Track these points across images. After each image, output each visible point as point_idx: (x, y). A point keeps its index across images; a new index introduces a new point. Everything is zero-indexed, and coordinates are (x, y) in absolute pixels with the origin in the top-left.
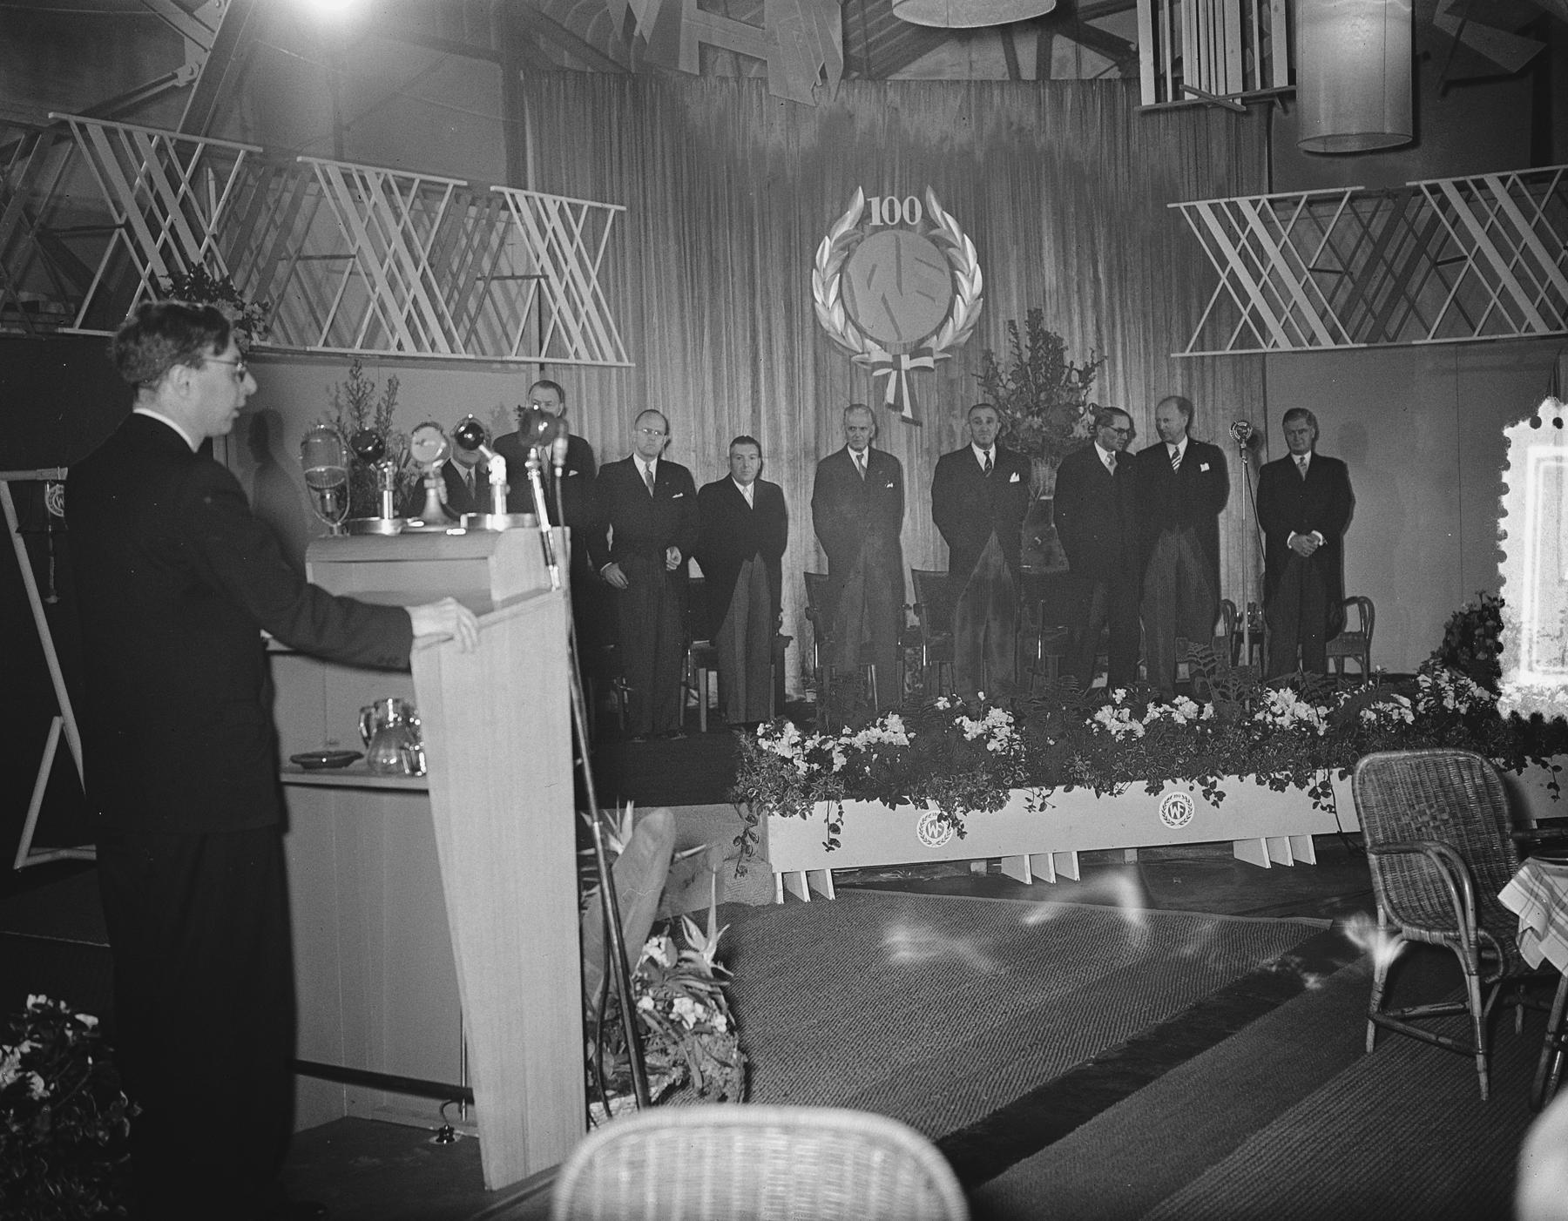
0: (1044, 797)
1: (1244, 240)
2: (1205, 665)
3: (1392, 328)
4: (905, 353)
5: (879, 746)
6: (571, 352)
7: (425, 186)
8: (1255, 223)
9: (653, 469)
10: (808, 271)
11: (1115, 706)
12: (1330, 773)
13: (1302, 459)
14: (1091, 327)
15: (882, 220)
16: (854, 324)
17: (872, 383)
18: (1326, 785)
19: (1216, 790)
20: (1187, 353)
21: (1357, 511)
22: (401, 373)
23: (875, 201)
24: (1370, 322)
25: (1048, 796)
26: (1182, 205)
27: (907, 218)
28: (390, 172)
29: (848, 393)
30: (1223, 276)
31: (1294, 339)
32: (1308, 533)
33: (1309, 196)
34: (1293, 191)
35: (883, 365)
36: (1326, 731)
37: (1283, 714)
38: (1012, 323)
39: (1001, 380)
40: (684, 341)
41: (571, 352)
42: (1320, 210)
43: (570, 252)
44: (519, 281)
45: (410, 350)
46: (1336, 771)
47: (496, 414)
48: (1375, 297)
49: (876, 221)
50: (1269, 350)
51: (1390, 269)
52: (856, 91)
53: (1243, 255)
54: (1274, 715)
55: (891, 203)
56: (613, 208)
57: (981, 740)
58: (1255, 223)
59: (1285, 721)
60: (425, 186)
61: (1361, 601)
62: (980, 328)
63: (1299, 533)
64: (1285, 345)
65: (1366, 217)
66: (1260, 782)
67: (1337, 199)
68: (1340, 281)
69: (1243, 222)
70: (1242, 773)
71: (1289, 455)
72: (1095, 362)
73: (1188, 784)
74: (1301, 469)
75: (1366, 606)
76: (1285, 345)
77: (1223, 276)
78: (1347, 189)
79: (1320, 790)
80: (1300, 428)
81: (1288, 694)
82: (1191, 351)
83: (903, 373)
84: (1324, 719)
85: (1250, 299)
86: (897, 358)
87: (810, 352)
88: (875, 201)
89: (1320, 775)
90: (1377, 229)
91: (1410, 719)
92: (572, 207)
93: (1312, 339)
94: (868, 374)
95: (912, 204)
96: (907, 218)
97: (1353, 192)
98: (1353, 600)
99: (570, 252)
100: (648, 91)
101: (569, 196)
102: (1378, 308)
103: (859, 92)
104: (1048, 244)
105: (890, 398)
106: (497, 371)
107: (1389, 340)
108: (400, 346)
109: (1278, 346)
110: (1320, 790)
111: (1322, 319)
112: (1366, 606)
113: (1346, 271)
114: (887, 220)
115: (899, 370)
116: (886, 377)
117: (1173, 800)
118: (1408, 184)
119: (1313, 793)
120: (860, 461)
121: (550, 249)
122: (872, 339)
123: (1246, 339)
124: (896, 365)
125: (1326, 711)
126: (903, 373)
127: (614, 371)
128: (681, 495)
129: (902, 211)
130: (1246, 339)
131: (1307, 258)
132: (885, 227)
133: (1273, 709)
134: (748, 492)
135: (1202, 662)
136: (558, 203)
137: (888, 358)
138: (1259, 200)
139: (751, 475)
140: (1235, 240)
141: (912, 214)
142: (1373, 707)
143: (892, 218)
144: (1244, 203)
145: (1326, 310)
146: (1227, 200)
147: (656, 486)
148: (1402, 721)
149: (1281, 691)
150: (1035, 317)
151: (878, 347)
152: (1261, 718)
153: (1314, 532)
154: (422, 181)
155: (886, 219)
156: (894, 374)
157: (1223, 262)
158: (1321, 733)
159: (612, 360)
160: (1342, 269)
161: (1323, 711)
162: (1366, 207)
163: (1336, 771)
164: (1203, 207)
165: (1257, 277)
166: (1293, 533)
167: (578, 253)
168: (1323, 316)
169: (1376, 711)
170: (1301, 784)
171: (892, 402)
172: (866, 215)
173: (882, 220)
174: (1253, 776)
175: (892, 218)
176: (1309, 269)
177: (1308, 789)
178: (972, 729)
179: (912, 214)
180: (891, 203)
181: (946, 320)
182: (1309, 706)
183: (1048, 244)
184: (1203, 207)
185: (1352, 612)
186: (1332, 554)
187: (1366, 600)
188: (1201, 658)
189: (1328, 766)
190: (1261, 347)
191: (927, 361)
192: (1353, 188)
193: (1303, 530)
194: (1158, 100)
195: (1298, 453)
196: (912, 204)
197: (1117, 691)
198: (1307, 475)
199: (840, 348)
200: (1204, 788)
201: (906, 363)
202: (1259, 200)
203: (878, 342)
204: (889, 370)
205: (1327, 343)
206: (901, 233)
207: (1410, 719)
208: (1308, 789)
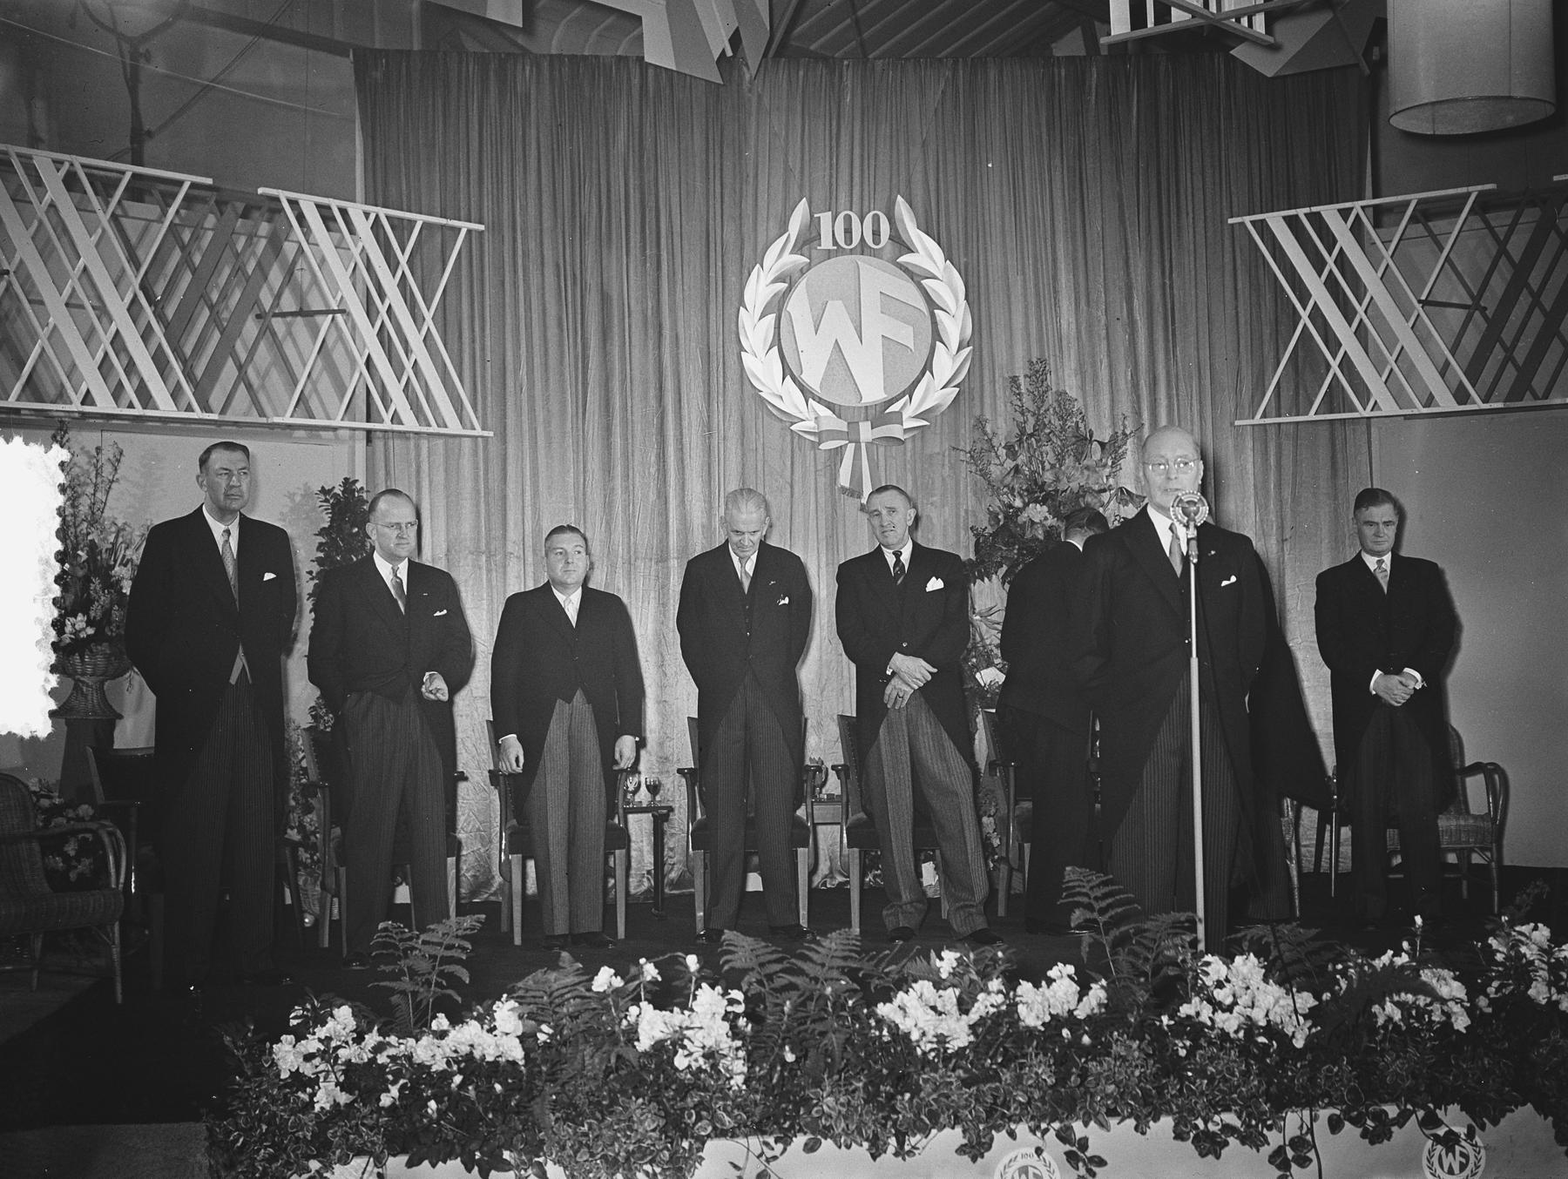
0: (768, 1160)
1: (1330, 261)
2: (1102, 911)
3: (1539, 382)
4: (866, 419)
5: (470, 1064)
6: (387, 417)
7: (196, 192)
8: (1345, 240)
9: (403, 574)
10: (734, 310)
11: (939, 985)
12: (1313, 1119)
13: (1380, 562)
14: (1123, 384)
15: (835, 243)
16: (794, 379)
17: (821, 459)
18: (1301, 1144)
19: (1089, 1153)
20: (1258, 420)
21: (1468, 638)
22: (134, 444)
23: (825, 218)
24: (1510, 373)
25: (775, 1158)
26: (1247, 220)
27: (869, 240)
28: (78, 161)
29: (788, 473)
30: (1305, 315)
31: (1399, 397)
32: (1399, 672)
33: (1420, 202)
34: (1396, 195)
35: (834, 435)
36: (1309, 1039)
37: (1230, 1009)
38: (1014, 379)
39: (998, 457)
40: (563, 404)
41: (387, 417)
42: (1437, 226)
43: (415, 339)
44: (289, 319)
45: (104, 403)
46: (1324, 1114)
47: (298, 499)
48: (1517, 339)
49: (826, 243)
50: (1367, 413)
51: (1536, 303)
52: (801, 73)
53: (1332, 285)
54: (1217, 1006)
55: (848, 219)
56: (465, 226)
57: (664, 1051)
58: (1345, 240)
59: (1229, 1023)
60: (196, 192)
61: (1489, 770)
62: (968, 390)
63: (1386, 672)
64: (1389, 407)
65: (1501, 232)
66: (1179, 1136)
67: (1458, 202)
68: (1469, 318)
69: (1330, 240)
70: (1144, 1117)
71: (1359, 556)
72: (1128, 432)
73: (1035, 1140)
74: (1380, 576)
75: (1496, 777)
76: (1389, 407)
77: (1305, 315)
78: (1471, 189)
79: (1290, 1153)
80: (1385, 519)
81: (1247, 966)
82: (1264, 416)
83: (863, 445)
84: (1306, 1017)
85: (1340, 345)
86: (854, 426)
87: (735, 417)
88: (825, 218)
89: (1293, 1121)
90: (1516, 247)
91: (1461, 1023)
92: (395, 223)
93: (1430, 401)
94: (815, 446)
95: (876, 219)
96: (869, 240)
97: (1481, 193)
98: (1477, 768)
99: (415, 339)
100: (519, 77)
101: (469, 221)
102: (1520, 355)
103: (806, 75)
104: (1064, 279)
105: (844, 479)
106: (298, 441)
107: (1536, 397)
108: (88, 399)
109: (1380, 409)
110: (1290, 1153)
111: (1443, 374)
112: (1496, 777)
113: (1475, 306)
114: (842, 243)
115: (858, 442)
116: (838, 453)
117: (1021, 1162)
118: (1556, 178)
119: (1278, 1159)
120: (743, 566)
121: (382, 334)
122: (820, 401)
123: (1335, 399)
124: (852, 435)
125: (1312, 1002)
126: (863, 445)
127: (467, 443)
128: (445, 612)
129: (862, 229)
130: (1335, 399)
131: (1416, 281)
132: (839, 251)
133: (1219, 995)
134: (571, 604)
135: (1097, 906)
136: (372, 217)
137: (842, 426)
138: (1352, 209)
139: (577, 575)
140: (1318, 264)
141: (876, 234)
142: (1396, 998)
143: (849, 240)
144: (1329, 213)
145: (1447, 363)
146: (1307, 210)
147: (408, 600)
148: (1447, 1024)
149: (1239, 959)
150: (1038, 373)
151: (829, 413)
152: (1193, 1013)
153: (1407, 670)
154: (135, 176)
155: (841, 241)
156: (851, 447)
157: (1304, 295)
158: (1299, 1043)
159: (454, 426)
160: (1470, 302)
161: (1306, 1001)
162: (1500, 220)
163: (1324, 1114)
164: (1276, 221)
165: (1348, 314)
166: (1378, 673)
167: (403, 284)
168: (1444, 370)
169: (1399, 1005)
170: (1252, 1139)
171: (847, 485)
172: (808, 240)
173: (835, 243)
174: (1167, 1122)
175: (849, 240)
176: (1419, 302)
177: (1266, 1150)
178: (651, 1025)
179: (876, 234)
180: (848, 219)
181: (923, 374)
182: (1283, 991)
183: (1064, 279)
184: (1276, 221)
185: (1475, 787)
186: (1431, 700)
187: (1496, 768)
188: (1096, 899)
189: (1310, 1102)
190: (1355, 410)
191: (895, 431)
192: (1480, 188)
193: (1393, 669)
194: (1134, 27)
195: (1373, 553)
196: (876, 219)
197: (945, 954)
198: (1390, 584)
199: (775, 412)
200: (1068, 1148)
201: (866, 432)
202: (1352, 209)
203: (830, 406)
204: (843, 443)
205: (1446, 403)
206: (864, 262)
207: (1461, 1023)
208: (1266, 1150)
